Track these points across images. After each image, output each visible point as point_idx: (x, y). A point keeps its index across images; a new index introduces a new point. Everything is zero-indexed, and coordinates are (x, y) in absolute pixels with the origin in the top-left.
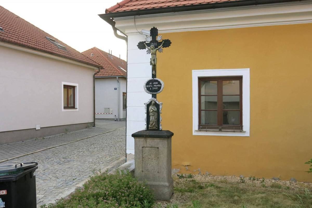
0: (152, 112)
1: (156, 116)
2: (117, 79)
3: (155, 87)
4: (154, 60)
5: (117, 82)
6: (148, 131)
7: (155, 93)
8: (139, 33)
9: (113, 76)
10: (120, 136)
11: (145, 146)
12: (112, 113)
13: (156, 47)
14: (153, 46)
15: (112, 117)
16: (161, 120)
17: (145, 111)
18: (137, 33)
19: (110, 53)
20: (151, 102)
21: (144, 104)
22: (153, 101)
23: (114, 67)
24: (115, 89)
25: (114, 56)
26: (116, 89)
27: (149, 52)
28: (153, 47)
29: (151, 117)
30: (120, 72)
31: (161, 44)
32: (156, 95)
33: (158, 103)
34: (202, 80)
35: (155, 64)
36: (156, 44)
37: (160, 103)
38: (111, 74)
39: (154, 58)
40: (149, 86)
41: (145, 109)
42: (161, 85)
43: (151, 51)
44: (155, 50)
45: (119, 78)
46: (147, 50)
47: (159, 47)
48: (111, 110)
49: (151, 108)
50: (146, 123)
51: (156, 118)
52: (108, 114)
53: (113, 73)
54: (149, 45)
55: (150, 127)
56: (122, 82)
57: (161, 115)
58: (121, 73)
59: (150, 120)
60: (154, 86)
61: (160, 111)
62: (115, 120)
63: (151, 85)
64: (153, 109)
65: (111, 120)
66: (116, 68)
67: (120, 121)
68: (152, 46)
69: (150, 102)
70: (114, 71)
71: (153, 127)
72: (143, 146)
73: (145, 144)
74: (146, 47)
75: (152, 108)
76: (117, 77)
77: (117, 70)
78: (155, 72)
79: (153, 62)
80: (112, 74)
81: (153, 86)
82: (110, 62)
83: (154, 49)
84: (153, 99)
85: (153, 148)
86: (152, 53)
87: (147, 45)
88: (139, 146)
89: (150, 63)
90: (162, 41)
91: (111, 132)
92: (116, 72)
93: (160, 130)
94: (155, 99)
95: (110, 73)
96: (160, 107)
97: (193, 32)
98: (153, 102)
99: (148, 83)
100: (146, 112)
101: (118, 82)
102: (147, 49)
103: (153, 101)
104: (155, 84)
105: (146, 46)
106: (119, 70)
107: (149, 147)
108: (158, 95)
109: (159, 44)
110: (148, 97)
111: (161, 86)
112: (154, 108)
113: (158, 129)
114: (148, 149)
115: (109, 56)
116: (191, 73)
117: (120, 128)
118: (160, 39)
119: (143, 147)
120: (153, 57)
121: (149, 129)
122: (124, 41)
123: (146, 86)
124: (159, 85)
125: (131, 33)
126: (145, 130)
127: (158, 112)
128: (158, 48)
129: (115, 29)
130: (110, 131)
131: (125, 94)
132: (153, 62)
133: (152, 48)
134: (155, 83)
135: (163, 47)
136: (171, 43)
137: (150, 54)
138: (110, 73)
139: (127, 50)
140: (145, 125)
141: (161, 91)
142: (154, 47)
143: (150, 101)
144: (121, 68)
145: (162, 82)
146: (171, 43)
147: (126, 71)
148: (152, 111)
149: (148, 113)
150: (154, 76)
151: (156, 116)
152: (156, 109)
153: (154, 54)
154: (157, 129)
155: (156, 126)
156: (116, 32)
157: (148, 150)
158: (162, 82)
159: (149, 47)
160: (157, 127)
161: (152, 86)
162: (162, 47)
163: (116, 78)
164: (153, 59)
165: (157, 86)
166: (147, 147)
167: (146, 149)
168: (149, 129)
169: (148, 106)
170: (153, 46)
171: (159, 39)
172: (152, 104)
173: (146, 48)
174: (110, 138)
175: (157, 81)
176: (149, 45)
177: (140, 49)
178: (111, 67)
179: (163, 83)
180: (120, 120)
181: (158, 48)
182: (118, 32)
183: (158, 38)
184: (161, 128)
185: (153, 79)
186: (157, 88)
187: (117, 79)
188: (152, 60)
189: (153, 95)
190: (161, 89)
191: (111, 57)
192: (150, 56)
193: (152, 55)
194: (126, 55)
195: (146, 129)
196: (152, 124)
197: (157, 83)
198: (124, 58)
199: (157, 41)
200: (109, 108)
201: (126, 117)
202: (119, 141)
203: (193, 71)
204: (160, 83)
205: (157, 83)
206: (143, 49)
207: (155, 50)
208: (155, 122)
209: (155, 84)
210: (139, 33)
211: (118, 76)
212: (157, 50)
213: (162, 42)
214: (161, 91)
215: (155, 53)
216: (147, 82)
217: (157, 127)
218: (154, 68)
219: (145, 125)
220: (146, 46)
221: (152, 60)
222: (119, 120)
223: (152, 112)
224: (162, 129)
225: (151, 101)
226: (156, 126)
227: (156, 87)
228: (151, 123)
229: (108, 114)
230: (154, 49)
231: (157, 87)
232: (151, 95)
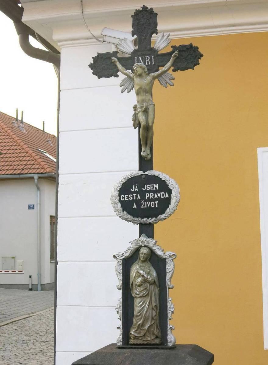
0: (140, 286)
1: (153, 299)
2: (36, 180)
3: (149, 200)
4: (146, 112)
5: (36, 189)
6: (127, 352)
7: (150, 220)
8: (95, 40)
9: (26, 174)
10: (41, 334)
12: (20, 268)
13: (151, 69)
14: (141, 67)
15: (22, 279)
16: (173, 312)
17: (117, 280)
18: (89, 41)
19: (20, 118)
20: (137, 251)
21: (114, 256)
22: (145, 246)
23: (6, 132)
24: (31, 207)
25: (30, 126)
26: (34, 208)
27: (127, 86)
28: (144, 69)
29: (138, 302)
30: (43, 163)
32: (151, 225)
33: (159, 252)
35: (150, 124)
36: (151, 60)
37: (168, 253)
38: (19, 169)
39: (145, 104)
40: (128, 197)
41: (114, 273)
42: (170, 192)
43: (137, 80)
44: (149, 78)
45: (39, 178)
46: (123, 81)
47: (162, 69)
48: (19, 261)
49: (138, 272)
50: (120, 323)
51: (154, 304)
52: (10, 272)
53: (26, 167)
54: (128, 62)
55: (135, 337)
56: (47, 189)
58: (46, 166)
59: (135, 313)
61: (168, 282)
62: (30, 287)
64: (143, 276)
65: (19, 289)
66: (34, 155)
67: (42, 290)
68: (139, 65)
69: (132, 249)
70: (29, 160)
71: (144, 335)
74: (118, 71)
75: (142, 272)
76: (36, 177)
77: (37, 157)
78: (148, 151)
79: (142, 118)
80: (23, 169)
82: (17, 138)
84: (143, 238)
86: (140, 88)
87: (120, 62)
89: (132, 122)
90: (171, 50)
91: (18, 323)
92: (33, 164)
93: (170, 345)
94: (150, 242)
95: (18, 167)
96: (169, 267)
98: (144, 251)
99: (125, 188)
100: (120, 283)
101: (38, 189)
102: (122, 76)
103: (145, 246)
104: (150, 192)
105: (120, 66)
106: (40, 158)
108: (157, 228)
109: (162, 58)
110: (126, 234)
111: (170, 196)
112: (147, 270)
113: (161, 343)
115: (16, 125)
116: (256, 154)
117: (41, 310)
118: (165, 44)
120: (141, 102)
121: (132, 342)
122: (50, 66)
123: (120, 195)
124: (163, 195)
125: (71, 40)
126: (119, 348)
127: (161, 285)
128: (159, 72)
129: (24, 31)
130: (14, 320)
131: (54, 220)
132: (142, 118)
133: (140, 71)
134: (148, 187)
135: (174, 71)
136: (202, 56)
137: (133, 92)
138: (18, 167)
139: (59, 91)
140: (118, 328)
141: (170, 215)
142: (146, 70)
143: (132, 247)
144: (47, 155)
145: (175, 184)
146: (202, 56)
147: (55, 160)
148: (139, 280)
149: (127, 287)
150: (145, 163)
151: (153, 299)
152: (154, 274)
153: (145, 92)
154: (157, 341)
155: (154, 334)
156: (28, 39)
158: (172, 183)
159: (127, 69)
160: (157, 337)
161: (139, 197)
162: (172, 68)
163: (33, 178)
164: (142, 107)
165: (156, 196)
168: (132, 342)
169: (127, 263)
170: (141, 67)
171: (159, 42)
172: (141, 256)
173: (119, 73)
174: (14, 342)
175: (156, 179)
176: (128, 62)
177: (99, 78)
178: (20, 151)
179: (177, 187)
180: (44, 288)
181: (159, 72)
182: (34, 42)
184: (173, 340)
185: (141, 172)
186: (157, 202)
187: (36, 180)
188: (139, 110)
189: (142, 225)
190: (172, 206)
191: (21, 128)
192: (132, 98)
193: (138, 94)
194: (56, 108)
195: (120, 344)
196: (143, 325)
197: (156, 187)
198: (51, 130)
199: (153, 51)
200: (13, 258)
201: (54, 281)
202: (38, 351)
203: (258, 149)
204: (167, 185)
205: (156, 187)
206: (108, 76)
207: (149, 78)
208: (153, 319)
209: (150, 192)
211: (38, 173)
212: (154, 78)
213: (173, 52)
214: (170, 215)
215: (147, 88)
216: (129, 180)
217: (159, 335)
218: (146, 138)
219: (118, 328)
220: (120, 66)
221: (139, 110)
222: (39, 288)
223: (140, 286)
224: (175, 342)
225: (136, 246)
226: (156, 333)
227: (155, 200)
228: (138, 322)
229: (10, 272)
230: (144, 74)
232: (137, 227)
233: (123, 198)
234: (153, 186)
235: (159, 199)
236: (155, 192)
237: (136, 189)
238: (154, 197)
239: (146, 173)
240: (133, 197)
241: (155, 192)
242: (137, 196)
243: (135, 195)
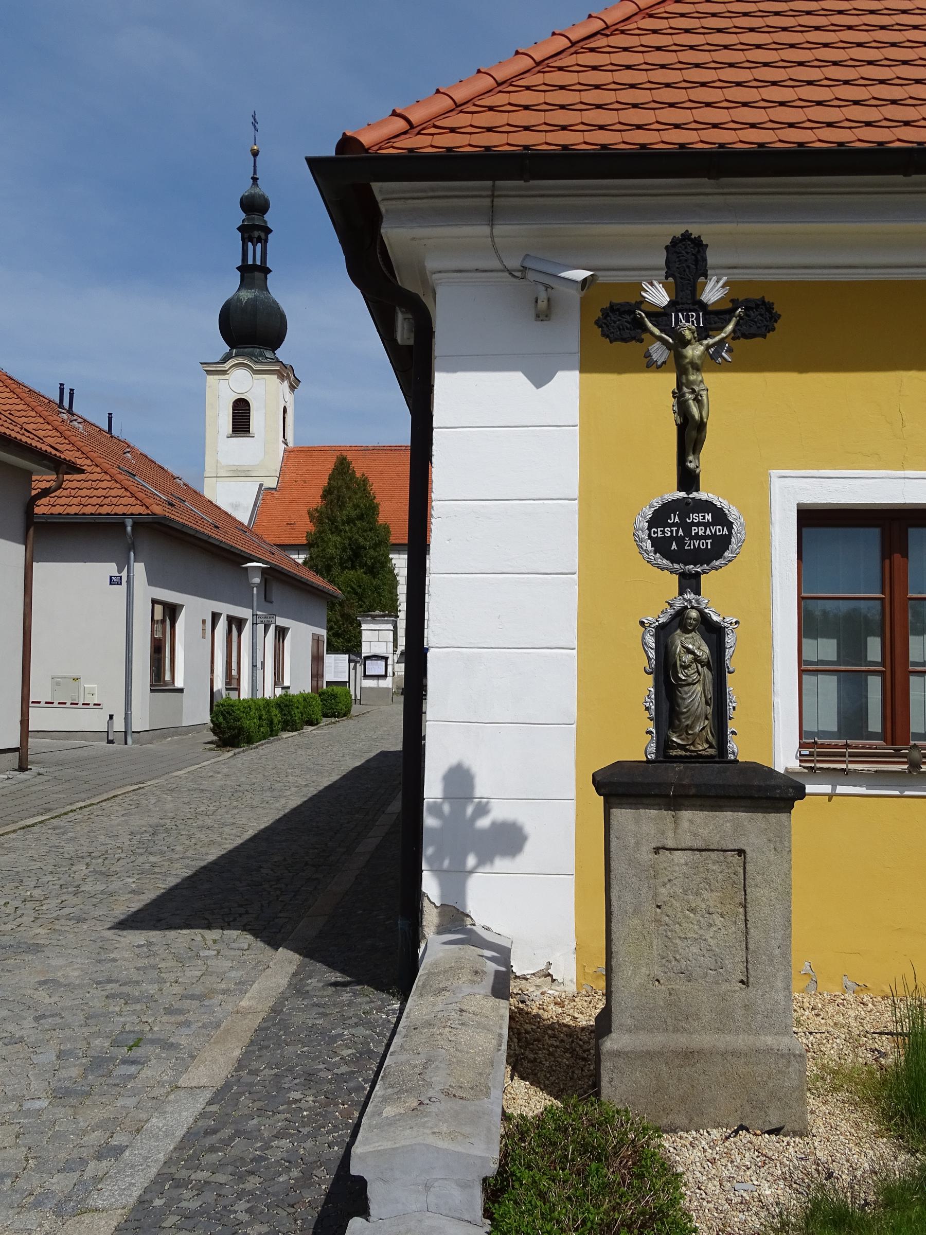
3: (697, 537)
8: (506, 274)
11: (670, 844)
28: (693, 333)
31: (730, 321)
34: (811, 519)
40: (663, 532)
42: (730, 525)
57: (731, 683)
60: (694, 530)
63: (673, 525)
72: (659, 845)
73: (670, 834)
81: (688, 532)
83: (693, 341)
85: (714, 855)
88: (637, 843)
93: (731, 757)
96: (729, 640)
97: (792, 283)
99: (659, 518)
104: (698, 524)
107: (713, 850)
114: (682, 861)
119: (657, 850)
123: (649, 529)
124: (719, 530)
127: (718, 666)
134: (695, 517)
140: (733, 733)
154: (712, 751)
157: (687, 864)
158: (733, 513)
161: (681, 533)
165: (708, 532)
166: (677, 850)
167: (676, 861)
171: (713, 292)
175: (707, 506)
183: (708, 288)
185: (683, 494)
186: (709, 541)
189: (683, 576)
197: (709, 517)
205: (709, 517)
209: (698, 524)
210: (510, 274)
226: (710, 737)
227: (706, 537)
230: (693, 341)
231: (708, 537)
233: (655, 533)
234: (704, 517)
235: (713, 536)
236: (706, 525)
237: (677, 520)
238: (705, 532)
239: (691, 496)
240: (672, 531)
241: (706, 525)
242: (677, 531)
243: (674, 529)
